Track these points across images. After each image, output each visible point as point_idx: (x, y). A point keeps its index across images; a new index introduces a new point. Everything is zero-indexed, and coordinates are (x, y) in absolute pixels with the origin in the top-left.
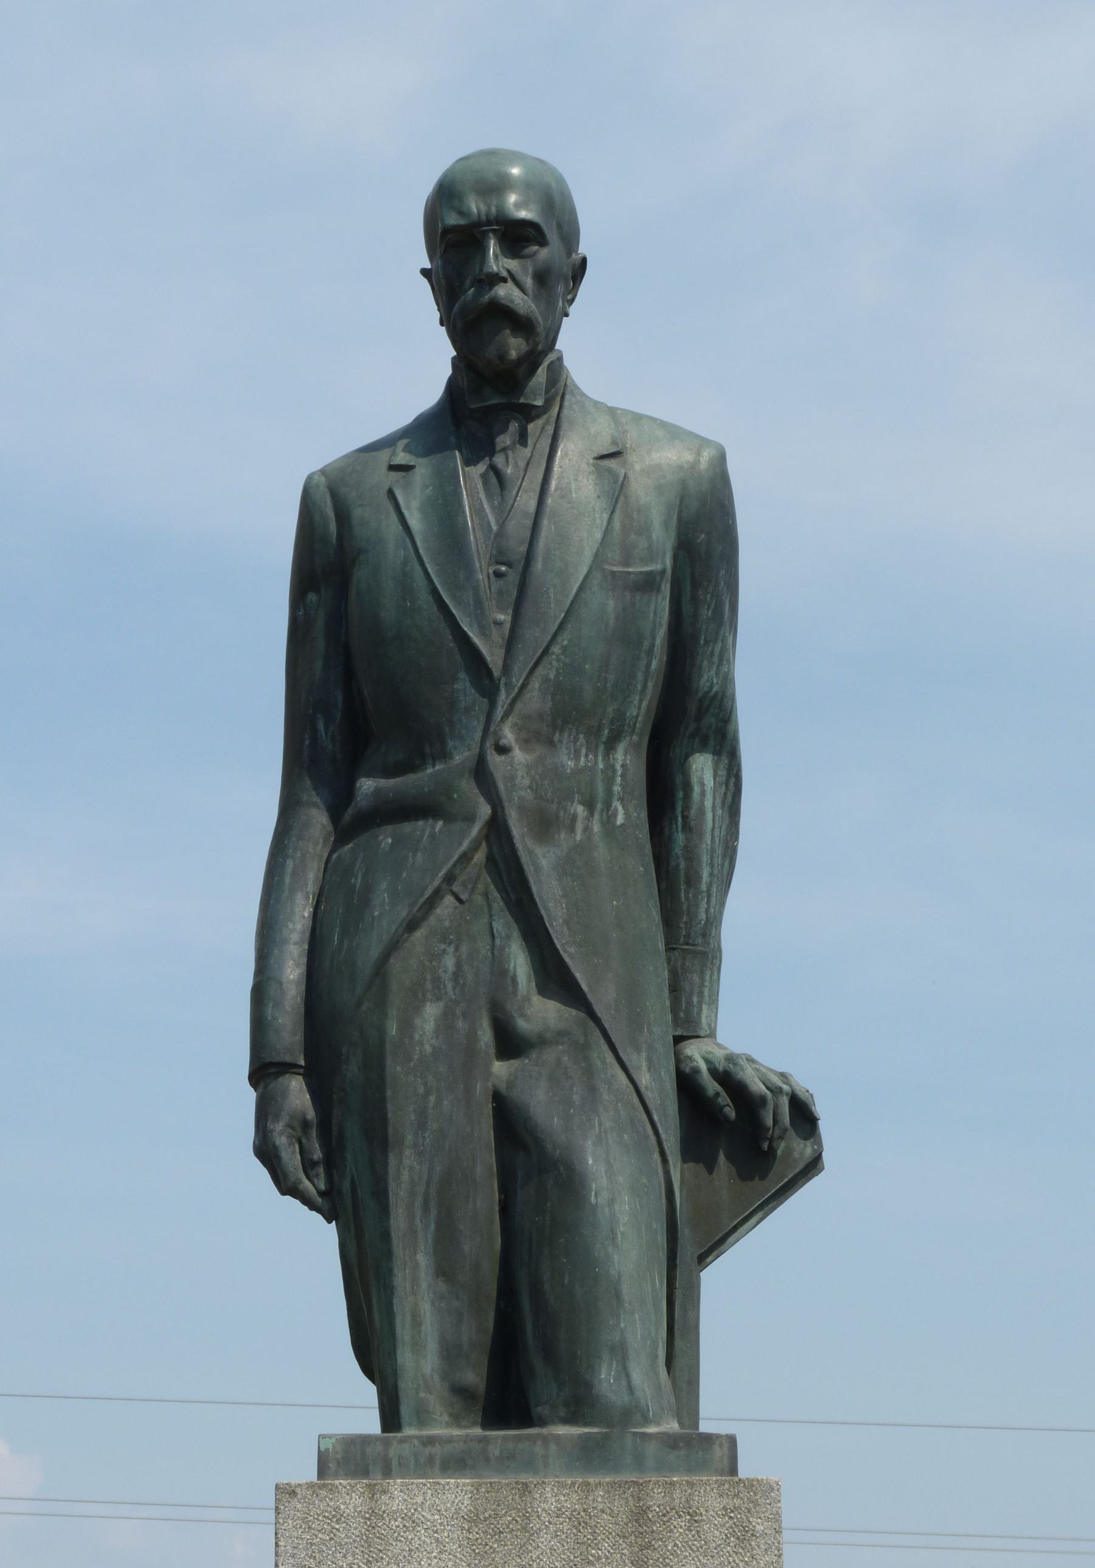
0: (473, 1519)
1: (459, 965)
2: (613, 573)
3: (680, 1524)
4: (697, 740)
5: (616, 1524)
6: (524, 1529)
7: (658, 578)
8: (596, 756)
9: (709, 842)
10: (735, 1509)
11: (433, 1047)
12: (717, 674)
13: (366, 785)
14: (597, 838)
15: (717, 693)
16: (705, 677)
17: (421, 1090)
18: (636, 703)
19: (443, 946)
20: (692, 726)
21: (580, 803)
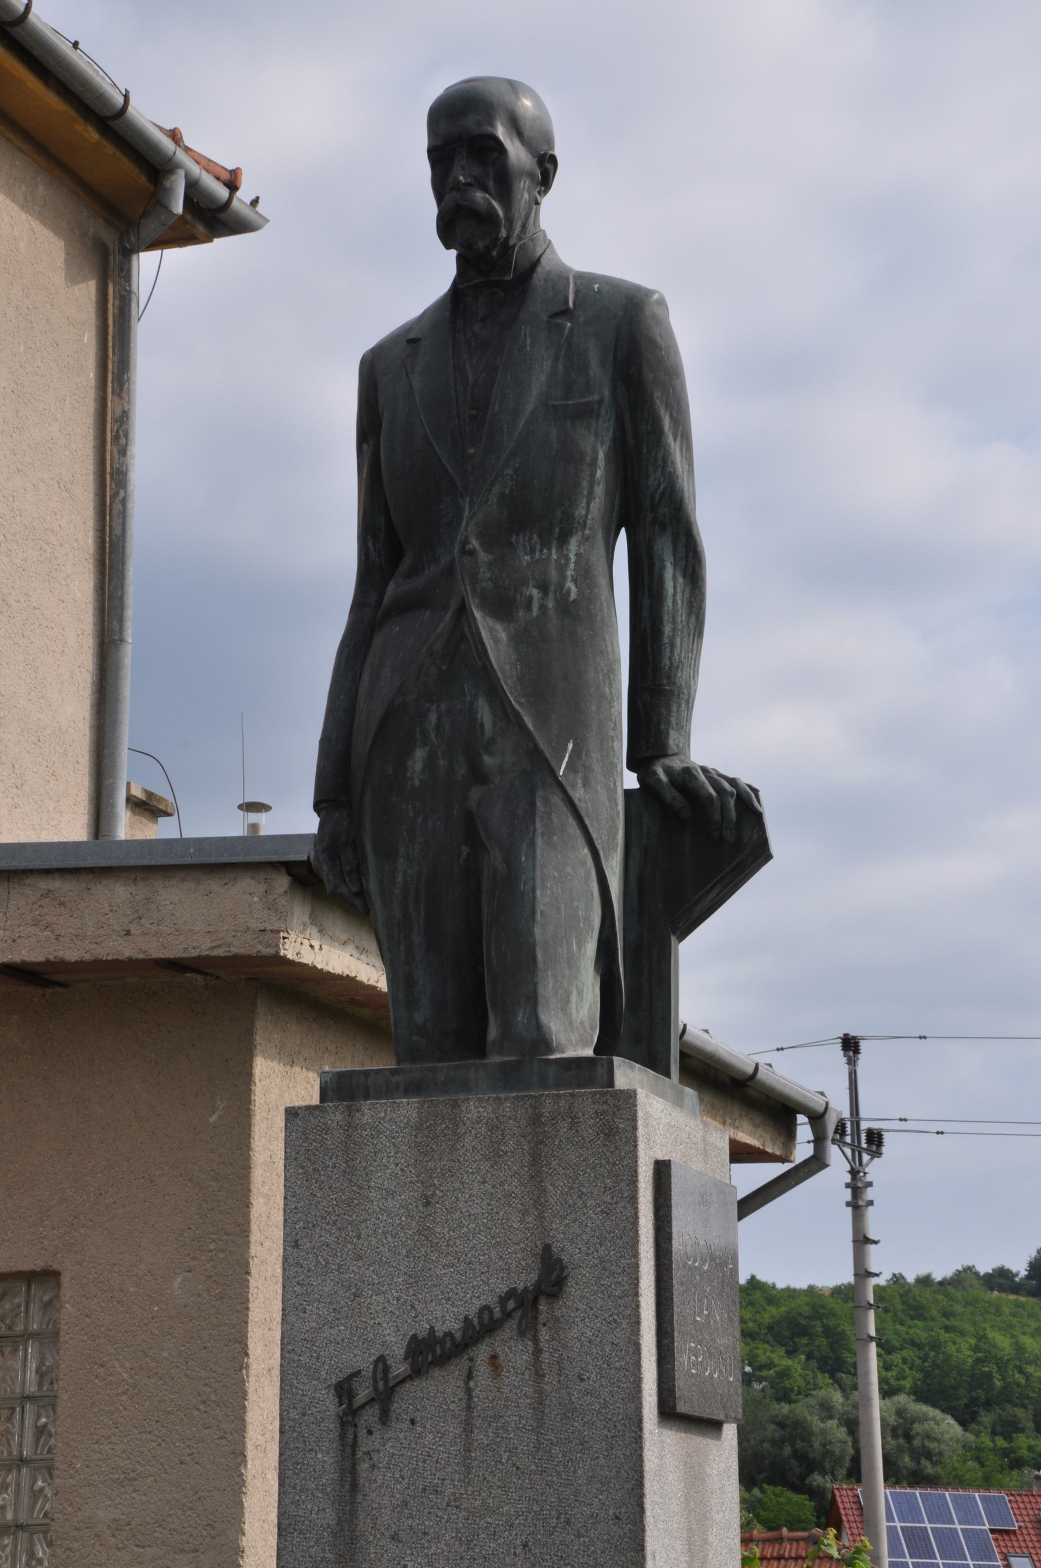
0: (419, 1128)
1: (439, 718)
2: (555, 407)
3: (564, 1127)
4: (657, 526)
5: (519, 1127)
6: (455, 1133)
7: (596, 406)
8: (550, 550)
9: (670, 605)
10: (605, 1112)
11: (420, 780)
12: (663, 474)
13: (391, 589)
14: (552, 613)
15: (665, 489)
16: (652, 478)
17: (411, 814)
18: (584, 505)
19: (428, 706)
20: (649, 519)
21: (534, 587)
